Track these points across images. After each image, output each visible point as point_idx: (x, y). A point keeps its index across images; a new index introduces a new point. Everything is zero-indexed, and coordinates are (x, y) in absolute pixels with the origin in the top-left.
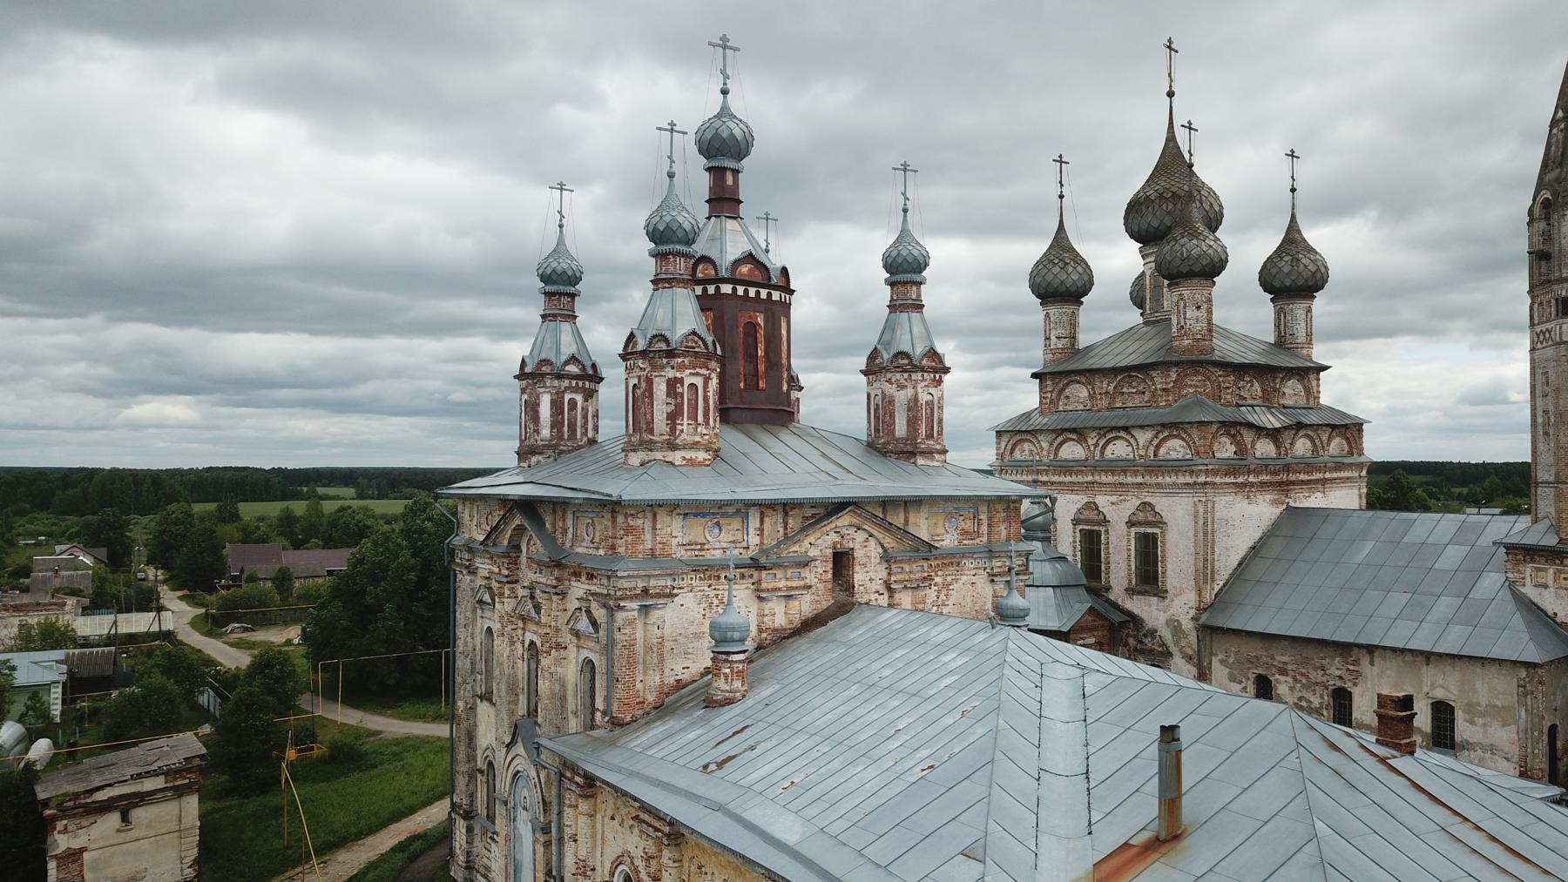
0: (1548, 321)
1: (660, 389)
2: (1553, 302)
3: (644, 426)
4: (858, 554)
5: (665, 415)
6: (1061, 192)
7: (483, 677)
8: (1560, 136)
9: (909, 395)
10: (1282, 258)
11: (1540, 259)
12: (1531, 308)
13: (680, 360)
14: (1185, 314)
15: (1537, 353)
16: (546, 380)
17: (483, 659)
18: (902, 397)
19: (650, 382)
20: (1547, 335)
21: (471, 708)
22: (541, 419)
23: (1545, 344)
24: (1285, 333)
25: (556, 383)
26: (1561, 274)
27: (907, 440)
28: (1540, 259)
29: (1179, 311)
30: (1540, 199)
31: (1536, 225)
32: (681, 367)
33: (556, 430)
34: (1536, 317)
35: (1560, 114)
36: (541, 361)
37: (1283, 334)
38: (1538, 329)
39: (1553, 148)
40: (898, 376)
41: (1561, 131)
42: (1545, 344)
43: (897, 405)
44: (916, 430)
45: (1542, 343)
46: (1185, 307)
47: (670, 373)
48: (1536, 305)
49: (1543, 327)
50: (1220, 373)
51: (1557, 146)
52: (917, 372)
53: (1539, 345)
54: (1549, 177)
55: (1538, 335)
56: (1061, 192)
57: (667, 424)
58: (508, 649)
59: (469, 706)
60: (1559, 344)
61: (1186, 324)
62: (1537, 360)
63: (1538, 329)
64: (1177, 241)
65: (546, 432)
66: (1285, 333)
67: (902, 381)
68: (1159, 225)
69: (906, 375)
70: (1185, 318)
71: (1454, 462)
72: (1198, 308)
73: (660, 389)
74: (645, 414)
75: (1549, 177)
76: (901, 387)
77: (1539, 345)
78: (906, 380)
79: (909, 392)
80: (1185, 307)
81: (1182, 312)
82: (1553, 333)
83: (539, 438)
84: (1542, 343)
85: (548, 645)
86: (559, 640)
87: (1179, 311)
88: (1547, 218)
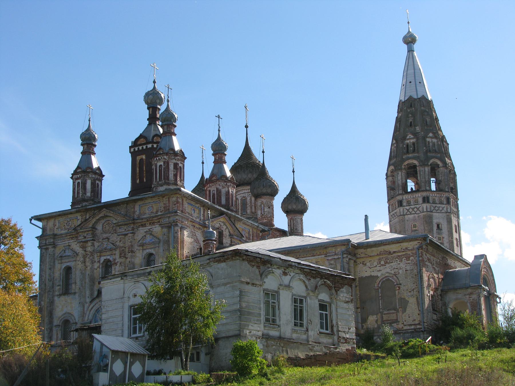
0: (396, 209)
1: (171, 167)
2: (397, 202)
3: (166, 178)
4: (224, 233)
5: (173, 175)
6: (203, 161)
7: (61, 287)
8: (395, 149)
9: (226, 190)
10: (292, 197)
11: (391, 190)
12: (389, 207)
13: (178, 157)
14: (264, 209)
15: (392, 222)
16: (89, 174)
17: (61, 280)
18: (224, 191)
19: (168, 163)
20: (395, 214)
21: (52, 302)
22: (87, 189)
23: (394, 218)
24: (293, 228)
25: (94, 176)
26: (399, 193)
27: (226, 205)
28: (391, 190)
29: (261, 209)
30: (390, 169)
31: (389, 178)
32: (178, 160)
33: (93, 194)
34: (391, 210)
35: (394, 142)
36: (89, 167)
37: (292, 229)
38: (392, 214)
39: (393, 153)
40: (223, 183)
41: (395, 147)
42: (394, 218)
43: (222, 193)
44: (229, 202)
45: (393, 218)
46: (264, 207)
47: (174, 161)
48: (391, 206)
49: (394, 212)
50: (278, 234)
51: (394, 152)
52: (229, 182)
53: (392, 219)
54: (392, 162)
55: (392, 216)
56: (203, 161)
57: (174, 178)
58: (91, 265)
59: (51, 301)
60: (400, 216)
61: (264, 213)
62: (392, 225)
63: (392, 214)
64: (261, 180)
65: (89, 194)
66: (293, 228)
67: (224, 185)
68: (246, 178)
69: (225, 183)
70: (264, 211)
71: (439, 121)
72: (269, 207)
73: (171, 167)
74: (166, 174)
75: (393, 161)
76: (223, 187)
77: (392, 219)
78: (225, 185)
79: (227, 189)
80: (264, 207)
81: (263, 209)
82: (397, 213)
83: (86, 196)
84: (393, 218)
85: (124, 254)
86: (133, 249)
87: (261, 209)
88: (393, 176)
